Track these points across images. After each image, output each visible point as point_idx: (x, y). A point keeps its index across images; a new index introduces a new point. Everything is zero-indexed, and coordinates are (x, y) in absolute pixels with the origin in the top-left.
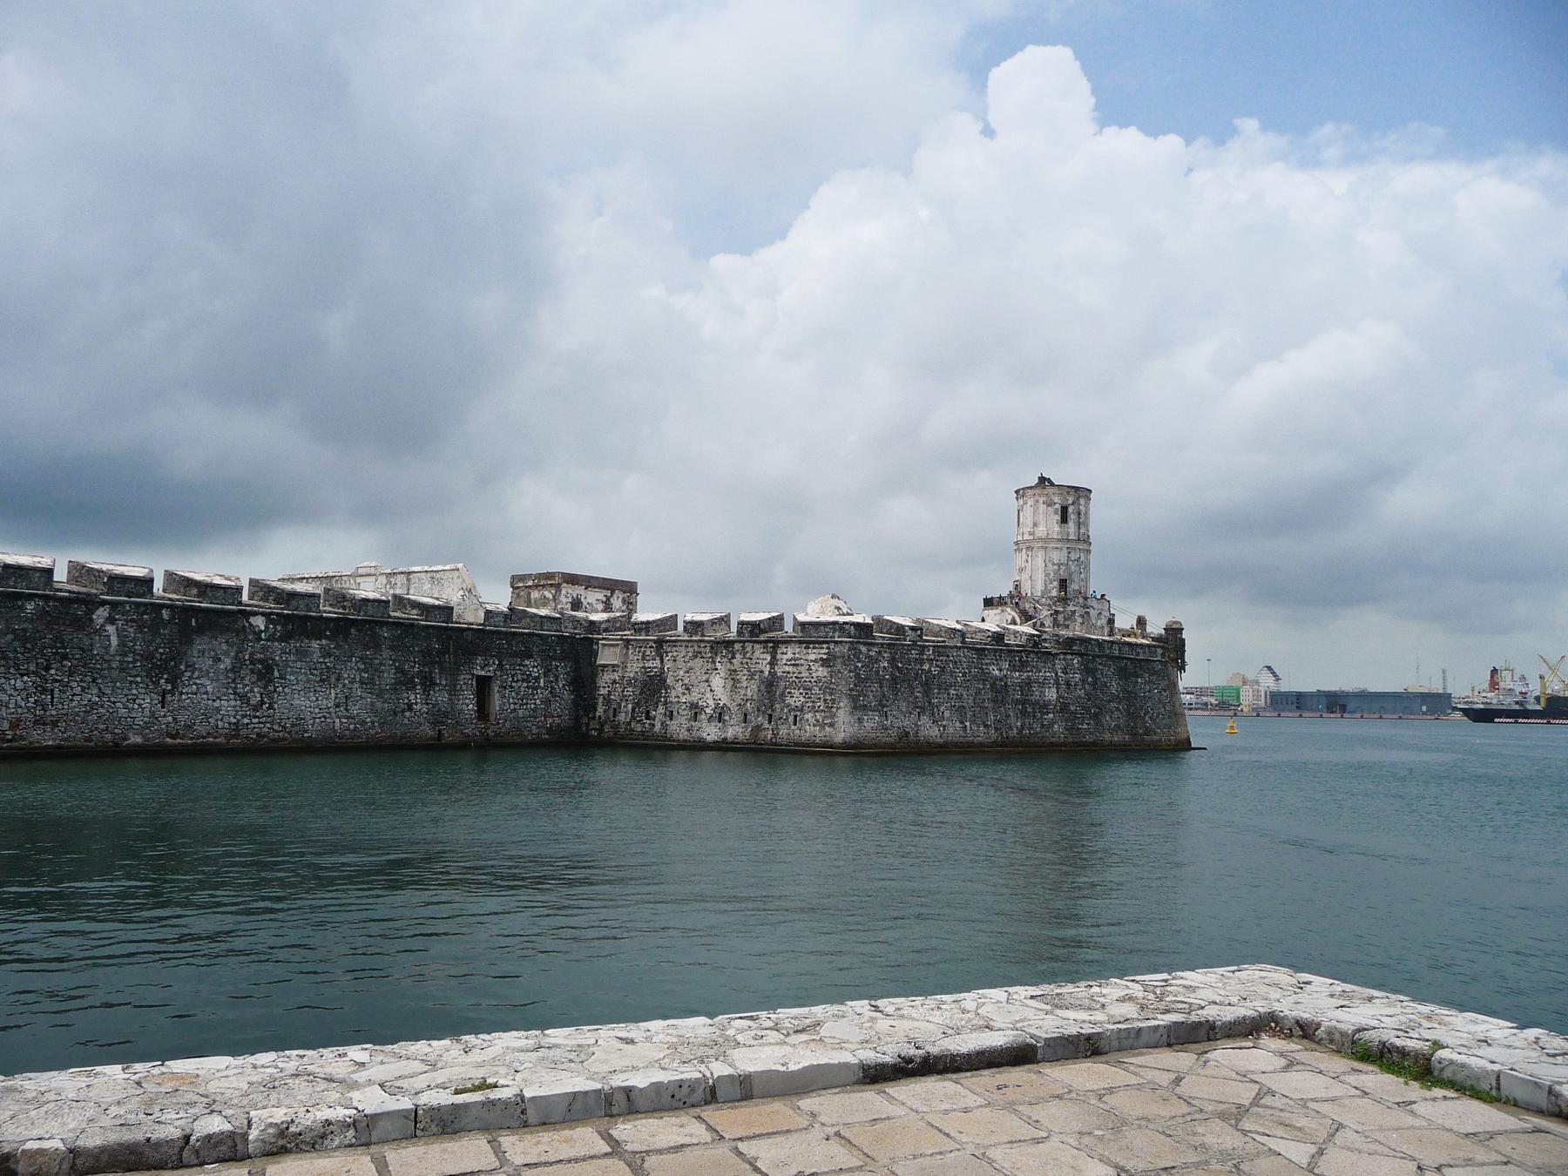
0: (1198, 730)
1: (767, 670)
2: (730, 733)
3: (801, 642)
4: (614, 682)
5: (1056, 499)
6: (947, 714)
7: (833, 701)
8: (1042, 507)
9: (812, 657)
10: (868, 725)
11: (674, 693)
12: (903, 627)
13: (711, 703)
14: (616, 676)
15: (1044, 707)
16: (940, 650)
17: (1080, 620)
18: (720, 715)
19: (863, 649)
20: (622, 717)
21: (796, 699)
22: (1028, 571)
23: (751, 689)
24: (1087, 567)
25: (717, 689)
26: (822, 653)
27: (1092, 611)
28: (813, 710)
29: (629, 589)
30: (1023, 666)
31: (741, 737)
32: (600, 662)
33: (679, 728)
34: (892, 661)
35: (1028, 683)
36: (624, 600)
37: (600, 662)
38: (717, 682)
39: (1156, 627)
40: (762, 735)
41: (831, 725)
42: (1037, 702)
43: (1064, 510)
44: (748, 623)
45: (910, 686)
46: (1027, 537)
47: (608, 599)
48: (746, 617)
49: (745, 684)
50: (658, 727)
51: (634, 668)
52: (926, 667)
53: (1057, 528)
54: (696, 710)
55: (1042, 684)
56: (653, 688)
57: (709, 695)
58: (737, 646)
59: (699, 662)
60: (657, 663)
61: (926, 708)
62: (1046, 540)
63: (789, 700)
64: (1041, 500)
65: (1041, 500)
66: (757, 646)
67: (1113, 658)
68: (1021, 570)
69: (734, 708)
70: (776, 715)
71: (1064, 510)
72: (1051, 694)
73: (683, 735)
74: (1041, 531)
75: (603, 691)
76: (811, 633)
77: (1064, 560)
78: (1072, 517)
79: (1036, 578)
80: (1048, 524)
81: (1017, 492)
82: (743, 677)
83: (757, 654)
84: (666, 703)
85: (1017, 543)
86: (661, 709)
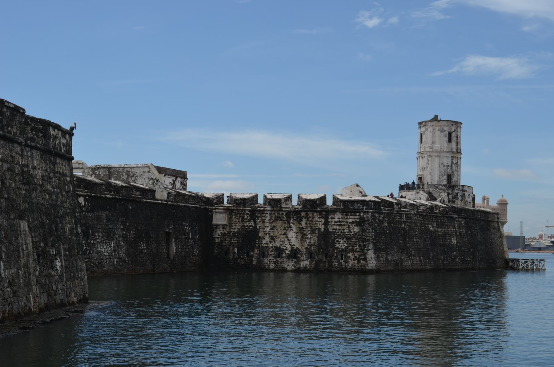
1: (323, 228)
5: (446, 128)
7: (365, 246)
8: (438, 133)
9: (350, 220)
11: (264, 242)
12: (392, 203)
13: (289, 247)
18: (295, 254)
19: (377, 215)
21: (342, 245)
22: (429, 169)
23: (312, 239)
27: (465, 193)
28: (353, 251)
29: (183, 175)
34: (389, 222)
35: (445, 234)
36: (181, 183)
37: (215, 222)
38: (292, 235)
43: (450, 134)
44: (310, 200)
46: (428, 149)
47: (174, 181)
49: (309, 236)
51: (237, 226)
52: (403, 226)
53: (446, 145)
54: (279, 252)
56: (250, 238)
57: (286, 242)
58: (303, 214)
59: (279, 223)
62: (440, 151)
63: (337, 245)
64: (437, 128)
65: (437, 128)
66: (315, 214)
71: (450, 134)
73: (272, 266)
74: (437, 146)
75: (217, 241)
76: (346, 207)
77: (450, 164)
78: (454, 139)
79: (434, 176)
80: (441, 143)
81: (420, 123)
83: (316, 219)
84: (259, 248)
86: (256, 251)
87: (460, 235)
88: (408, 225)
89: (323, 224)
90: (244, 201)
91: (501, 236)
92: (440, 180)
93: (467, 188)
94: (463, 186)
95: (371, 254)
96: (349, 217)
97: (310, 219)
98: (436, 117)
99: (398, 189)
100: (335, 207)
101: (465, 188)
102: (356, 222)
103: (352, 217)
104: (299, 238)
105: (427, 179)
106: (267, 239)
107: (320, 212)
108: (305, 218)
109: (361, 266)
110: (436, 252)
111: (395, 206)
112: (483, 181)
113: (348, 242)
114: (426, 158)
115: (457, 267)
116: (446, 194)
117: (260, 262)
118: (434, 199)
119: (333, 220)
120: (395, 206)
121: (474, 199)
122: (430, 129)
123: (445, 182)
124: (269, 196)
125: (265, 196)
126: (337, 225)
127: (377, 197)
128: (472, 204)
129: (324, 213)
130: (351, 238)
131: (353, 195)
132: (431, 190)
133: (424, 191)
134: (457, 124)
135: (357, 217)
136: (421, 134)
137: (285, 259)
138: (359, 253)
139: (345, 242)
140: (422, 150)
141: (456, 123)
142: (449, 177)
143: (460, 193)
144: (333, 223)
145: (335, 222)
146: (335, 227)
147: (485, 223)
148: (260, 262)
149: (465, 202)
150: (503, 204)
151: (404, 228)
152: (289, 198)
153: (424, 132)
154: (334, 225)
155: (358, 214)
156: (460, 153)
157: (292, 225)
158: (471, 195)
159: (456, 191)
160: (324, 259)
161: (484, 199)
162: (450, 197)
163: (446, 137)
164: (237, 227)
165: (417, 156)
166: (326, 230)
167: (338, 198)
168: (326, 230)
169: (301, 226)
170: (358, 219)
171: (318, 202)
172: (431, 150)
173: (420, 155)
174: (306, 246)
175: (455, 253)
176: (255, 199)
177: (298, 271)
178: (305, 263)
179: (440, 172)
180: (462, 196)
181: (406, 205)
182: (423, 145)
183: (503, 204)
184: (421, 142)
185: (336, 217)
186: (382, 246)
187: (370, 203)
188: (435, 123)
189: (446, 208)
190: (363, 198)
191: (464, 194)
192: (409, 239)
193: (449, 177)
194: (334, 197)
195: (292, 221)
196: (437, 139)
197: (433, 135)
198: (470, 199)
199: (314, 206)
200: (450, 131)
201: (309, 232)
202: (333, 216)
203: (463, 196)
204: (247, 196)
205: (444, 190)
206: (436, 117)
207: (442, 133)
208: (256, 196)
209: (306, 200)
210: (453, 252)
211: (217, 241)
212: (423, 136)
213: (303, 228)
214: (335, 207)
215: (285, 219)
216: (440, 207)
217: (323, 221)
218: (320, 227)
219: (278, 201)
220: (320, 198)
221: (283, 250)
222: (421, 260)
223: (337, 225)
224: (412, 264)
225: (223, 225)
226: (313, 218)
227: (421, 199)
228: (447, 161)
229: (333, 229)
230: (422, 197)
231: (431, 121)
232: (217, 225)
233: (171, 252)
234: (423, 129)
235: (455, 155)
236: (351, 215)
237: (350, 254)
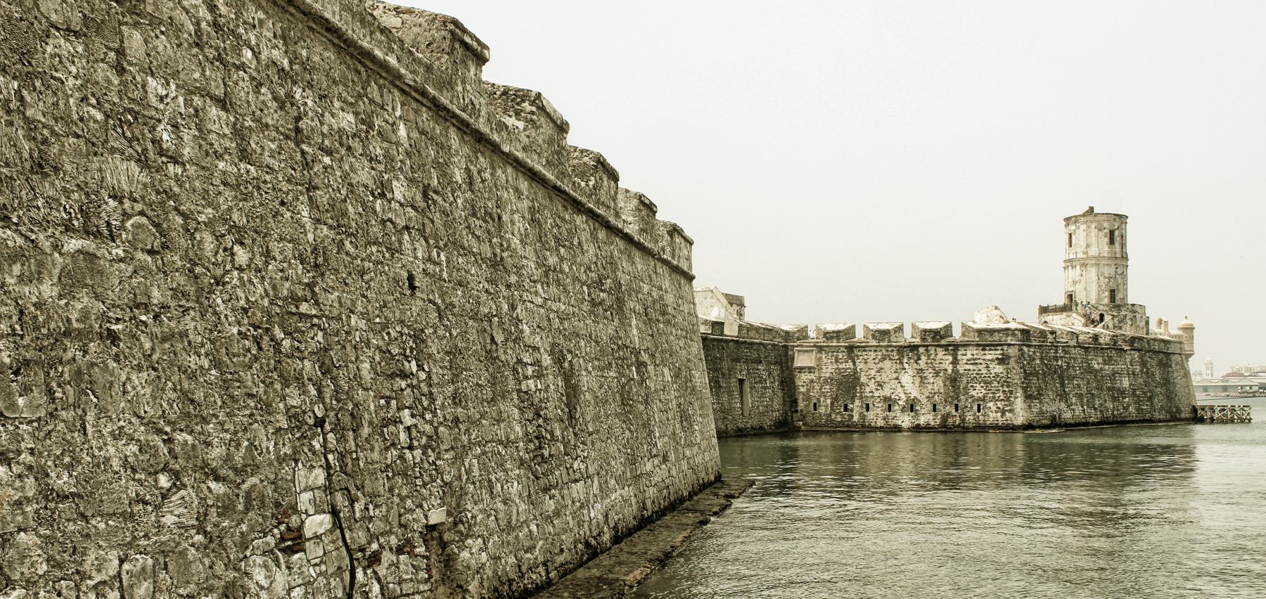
1: (950, 368)
2: (922, 420)
3: (978, 345)
4: (812, 381)
5: (1106, 225)
7: (1011, 392)
8: (1094, 231)
9: (989, 357)
11: (868, 389)
13: (903, 396)
14: (812, 376)
15: (1122, 392)
16: (1066, 348)
18: (911, 407)
19: (1026, 349)
20: (822, 410)
21: (978, 391)
23: (938, 384)
24: (519, 90)
25: (907, 384)
26: (997, 353)
28: (994, 399)
31: (932, 423)
32: (797, 364)
33: (876, 416)
34: (1042, 359)
37: (797, 364)
38: (906, 379)
40: (950, 420)
41: (1011, 411)
44: (930, 331)
46: (1080, 255)
49: (931, 380)
50: (856, 418)
51: (828, 370)
54: (889, 403)
56: (849, 385)
57: (900, 390)
58: (922, 350)
59: (887, 364)
60: (850, 365)
62: (1098, 258)
63: (972, 392)
67: (1154, 351)
68: (1075, 283)
69: (924, 400)
70: (961, 404)
71: (1112, 233)
72: (1126, 383)
73: (880, 423)
74: (1093, 251)
75: (802, 390)
76: (986, 339)
77: (1113, 274)
78: (1117, 239)
79: (1090, 290)
80: (1100, 246)
81: (1067, 220)
82: (929, 374)
84: (861, 398)
85: (1070, 261)
86: (857, 402)
90: (837, 335)
95: (1019, 404)
98: (1092, 209)
101: (1137, 309)
104: (917, 383)
105: (1080, 297)
106: (872, 385)
107: (946, 347)
110: (1096, 405)
112: (1160, 301)
117: (863, 417)
121: (1147, 323)
122: (1083, 227)
123: (1106, 301)
124: (872, 327)
125: (964, 326)
130: (990, 383)
133: (1078, 314)
134: (1122, 218)
137: (899, 414)
141: (1120, 216)
142: (1113, 293)
146: (968, 367)
147: (1162, 357)
148: (863, 417)
149: (1137, 327)
150: (1189, 329)
152: (899, 329)
157: (906, 366)
159: (1123, 313)
160: (954, 412)
161: (1160, 322)
164: (829, 370)
166: (955, 371)
168: (955, 371)
176: (850, 332)
177: (917, 429)
178: (926, 418)
179: (1100, 286)
182: (1073, 250)
185: (969, 353)
188: (1090, 218)
190: (1005, 326)
194: (964, 326)
198: (1143, 323)
199: (937, 338)
203: (1133, 319)
204: (841, 327)
206: (1092, 209)
208: (853, 327)
209: (925, 331)
211: (802, 390)
217: (950, 358)
219: (884, 333)
221: (895, 401)
225: (810, 368)
227: (1074, 323)
228: (1109, 271)
230: (1076, 322)
231: (1084, 215)
232: (801, 369)
233: (745, 407)
234: (1072, 227)
235: (1119, 262)
237: (990, 404)
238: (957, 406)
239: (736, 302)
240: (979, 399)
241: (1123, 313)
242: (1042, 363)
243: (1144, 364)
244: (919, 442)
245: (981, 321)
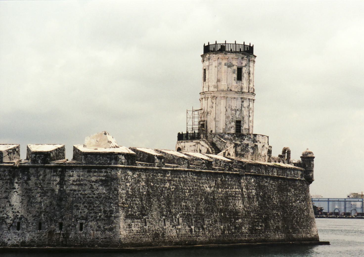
0: (322, 227)
2: (28, 237)
3: (84, 168)
5: (235, 62)
6: (181, 220)
9: (93, 179)
10: (135, 229)
13: (11, 214)
15: (235, 214)
17: (251, 151)
19: (130, 173)
28: (95, 219)
30: (223, 185)
34: (147, 181)
38: (15, 199)
39: (296, 157)
42: (231, 211)
43: (239, 71)
44: (41, 153)
45: (159, 200)
46: (212, 89)
48: (35, 148)
49: (39, 199)
52: (167, 185)
55: (234, 197)
61: (170, 216)
64: (224, 62)
65: (224, 62)
69: (30, 219)
70: (65, 223)
71: (239, 71)
72: (240, 205)
74: (223, 85)
77: (239, 107)
83: (48, 176)
85: (203, 93)
87: (249, 197)
88: (174, 185)
89: (58, 184)
91: (306, 198)
92: (226, 128)
93: (261, 137)
94: (255, 135)
96: (92, 174)
97: (41, 177)
99: (177, 138)
100: (74, 162)
102: (101, 180)
103: (95, 174)
104: (25, 202)
108: (34, 176)
109: (105, 238)
111: (157, 160)
112: (279, 131)
113: (90, 206)
114: (210, 99)
115: (243, 238)
116: (233, 145)
118: (218, 151)
119: (71, 178)
120: (157, 160)
121: (270, 152)
122: (215, 64)
123: (233, 131)
125: (75, 149)
126: (77, 185)
127: (134, 150)
128: (267, 157)
129: (59, 170)
131: (99, 146)
132: (215, 140)
135: (102, 174)
136: (205, 70)
138: (103, 222)
139: (85, 207)
140: (206, 89)
143: (251, 144)
144: (71, 182)
145: (74, 181)
146: (74, 187)
150: (307, 160)
151: (169, 189)
153: (209, 66)
154: (73, 184)
155: (103, 170)
156: (253, 93)
157: (16, 186)
158: (266, 146)
159: (246, 142)
162: (239, 149)
163: (234, 73)
165: (200, 97)
167: (79, 150)
169: (28, 187)
170: (104, 176)
171: (52, 155)
172: (216, 90)
173: (203, 96)
174: (34, 213)
175: (240, 220)
179: (227, 117)
180: (253, 148)
181: (174, 158)
183: (307, 160)
184: (205, 80)
186: (135, 212)
187: (120, 157)
189: (229, 162)
191: (256, 146)
192: (176, 202)
193: (239, 124)
195: (16, 181)
196: (223, 77)
197: (218, 71)
198: (265, 152)
200: (240, 65)
201: (39, 195)
202: (71, 173)
203: (255, 148)
205: (231, 140)
207: (229, 69)
209: (36, 153)
210: (238, 219)
212: (207, 72)
213: (30, 190)
214: (74, 162)
215: (8, 177)
216: (221, 161)
217: (58, 179)
218: (54, 187)
220: (56, 150)
222: (191, 230)
223: (77, 185)
224: (178, 235)
226: (45, 176)
229: (71, 190)
234: (207, 63)
236: (95, 172)
238: (61, 225)
239: (224, 126)
240: (83, 218)
241: (246, 142)
242: (148, 185)
243: (260, 187)
244: (316, 236)
245: (88, 146)
